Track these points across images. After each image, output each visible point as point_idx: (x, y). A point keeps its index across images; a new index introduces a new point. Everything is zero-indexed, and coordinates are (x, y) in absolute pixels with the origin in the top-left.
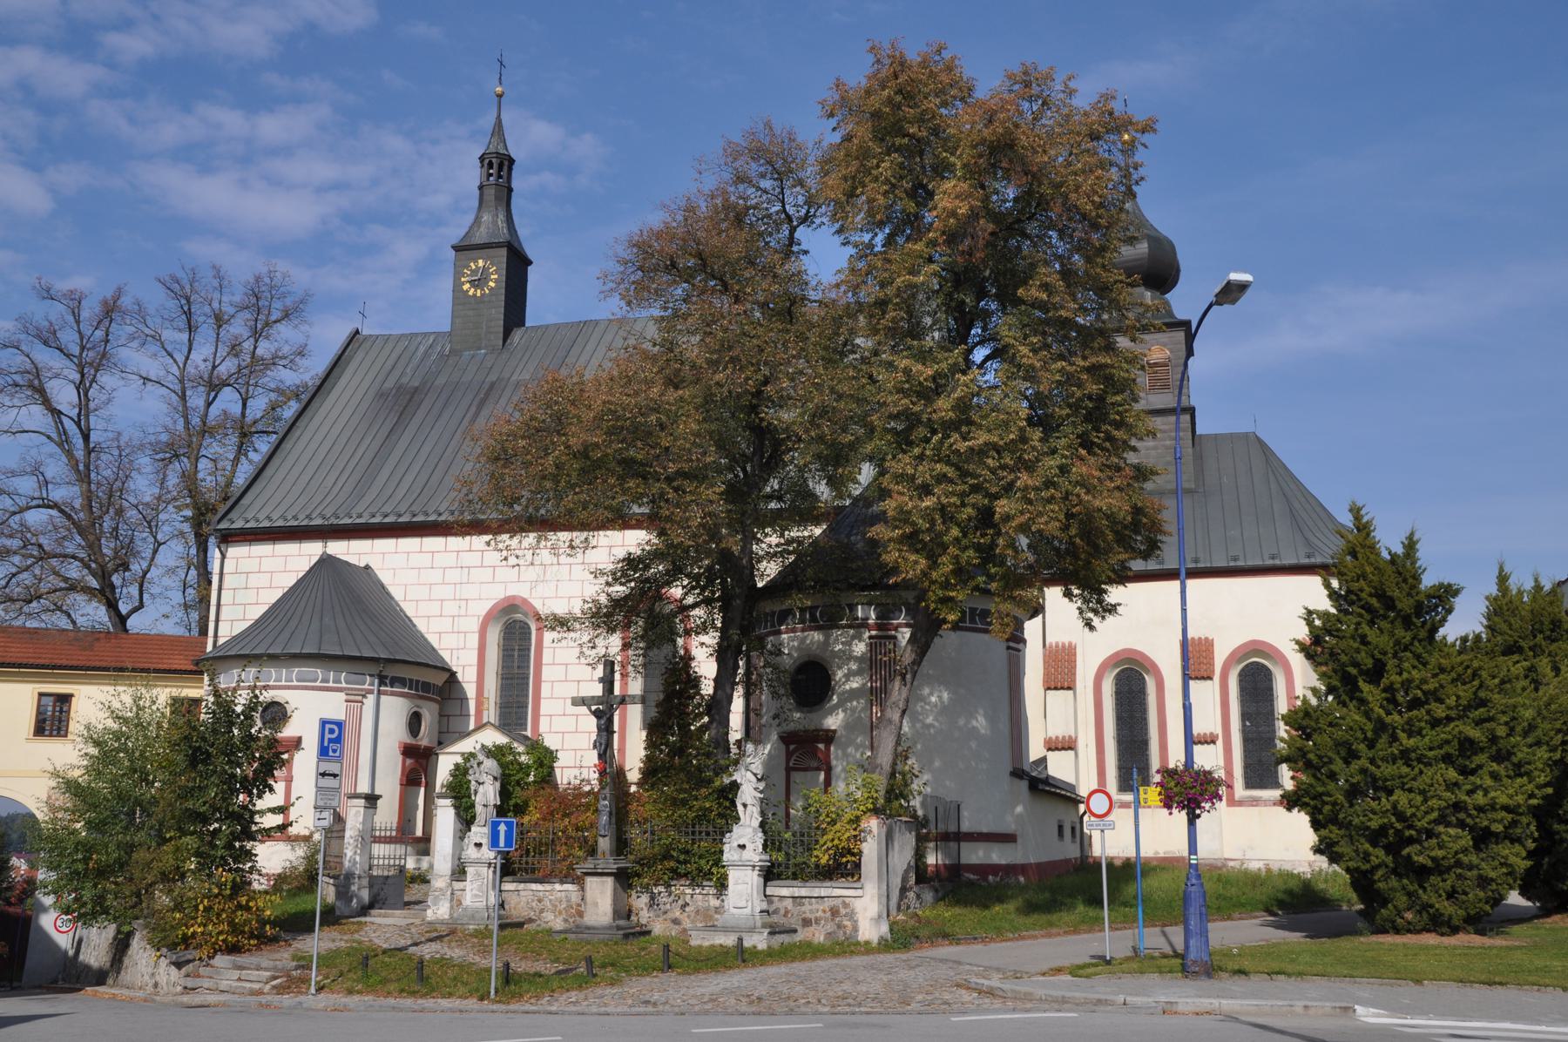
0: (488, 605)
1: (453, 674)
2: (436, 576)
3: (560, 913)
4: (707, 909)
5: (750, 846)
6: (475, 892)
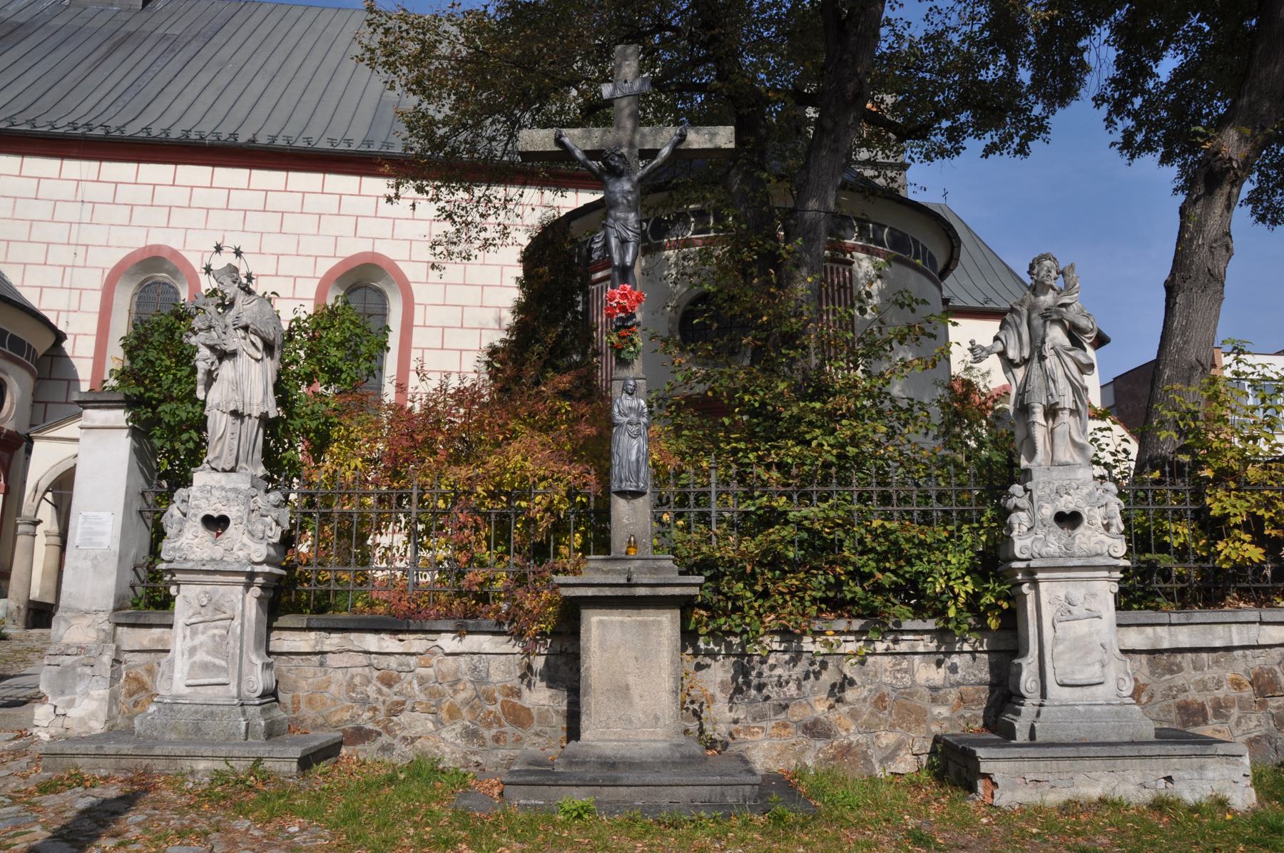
0: (120, 255)
1: (60, 337)
2: (41, 210)
3: (454, 713)
4: (909, 693)
5: (1094, 516)
6: (201, 656)
